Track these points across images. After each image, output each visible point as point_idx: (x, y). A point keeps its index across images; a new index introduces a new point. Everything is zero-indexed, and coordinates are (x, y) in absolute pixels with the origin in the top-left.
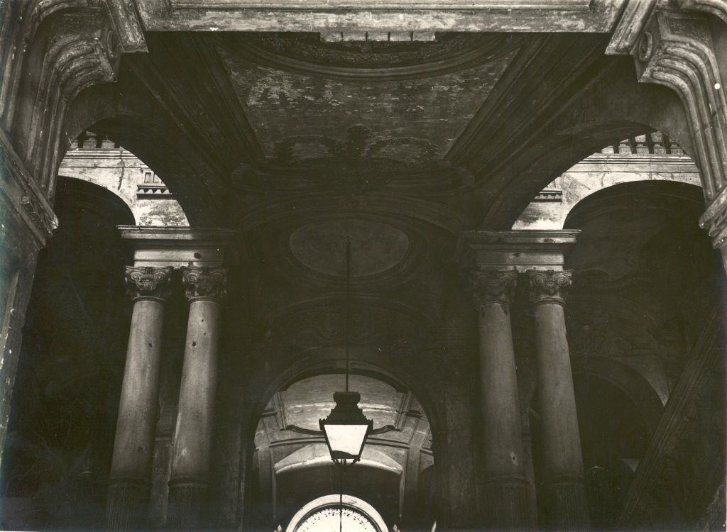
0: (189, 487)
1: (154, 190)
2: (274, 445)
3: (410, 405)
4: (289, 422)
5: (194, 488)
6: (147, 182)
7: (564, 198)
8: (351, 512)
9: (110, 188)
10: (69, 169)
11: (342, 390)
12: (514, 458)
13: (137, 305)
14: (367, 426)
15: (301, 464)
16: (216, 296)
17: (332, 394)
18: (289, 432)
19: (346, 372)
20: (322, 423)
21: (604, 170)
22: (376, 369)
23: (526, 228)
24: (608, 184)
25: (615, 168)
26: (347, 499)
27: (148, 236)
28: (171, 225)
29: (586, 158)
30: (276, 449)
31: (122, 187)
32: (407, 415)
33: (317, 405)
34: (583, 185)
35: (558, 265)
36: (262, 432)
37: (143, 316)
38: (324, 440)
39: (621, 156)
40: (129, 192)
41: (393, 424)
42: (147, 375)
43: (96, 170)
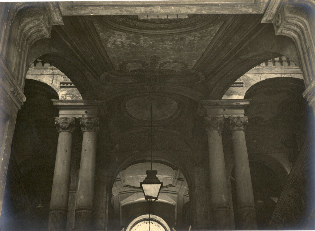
1: (67, 84)
2: (120, 193)
3: (179, 175)
4: (127, 184)
6: (64, 81)
7: (244, 85)
8: (154, 222)
9: (48, 84)
10: (30, 76)
11: (150, 169)
12: (224, 198)
13: (60, 134)
14: (160, 185)
15: (132, 201)
19: (151, 161)
20: (141, 184)
22: (164, 160)
23: (228, 98)
24: (263, 79)
26: (152, 216)
27: (65, 104)
28: (74, 99)
30: (121, 195)
31: (53, 83)
33: (139, 176)
37: (64, 139)
38: (142, 191)
39: (269, 67)
41: (171, 184)
42: (65, 165)
43: (42, 76)
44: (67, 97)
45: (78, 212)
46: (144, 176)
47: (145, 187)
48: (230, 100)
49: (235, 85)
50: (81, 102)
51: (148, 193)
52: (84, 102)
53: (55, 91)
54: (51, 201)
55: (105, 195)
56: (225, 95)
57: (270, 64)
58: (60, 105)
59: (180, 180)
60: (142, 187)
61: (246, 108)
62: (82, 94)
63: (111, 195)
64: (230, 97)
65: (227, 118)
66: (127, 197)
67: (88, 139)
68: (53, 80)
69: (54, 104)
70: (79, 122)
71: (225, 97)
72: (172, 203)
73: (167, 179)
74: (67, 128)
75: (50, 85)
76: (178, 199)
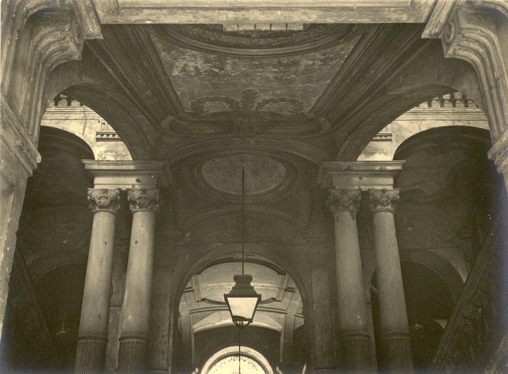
0: (133, 342)
1: (108, 135)
2: (192, 312)
4: (203, 296)
5: (137, 342)
7: (393, 138)
9: (77, 134)
12: (360, 320)
15: (211, 325)
16: (151, 209)
18: (203, 303)
19: (242, 261)
20: (226, 296)
23: (367, 160)
24: (424, 129)
26: (244, 349)
28: (119, 159)
29: (408, 110)
30: (194, 315)
31: (85, 133)
32: (285, 290)
40: (90, 137)
43: (67, 121)
47: (232, 301)
50: (129, 164)
51: (236, 313)
52: (135, 164)
57: (436, 105)
59: (288, 291)
60: (227, 303)
61: (396, 175)
70: (87, 198)
71: (362, 158)
74: (108, 207)
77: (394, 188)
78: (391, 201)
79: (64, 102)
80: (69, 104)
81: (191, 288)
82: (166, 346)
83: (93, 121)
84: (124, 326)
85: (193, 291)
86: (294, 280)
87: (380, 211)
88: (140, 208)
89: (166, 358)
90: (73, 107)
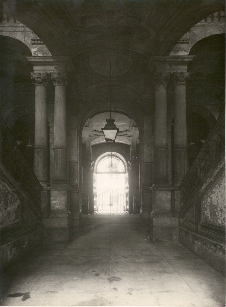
1: (38, 41)
2: (90, 136)
3: (133, 123)
4: (94, 129)
5: (61, 151)
6: (35, 38)
7: (190, 42)
8: (115, 157)
9: (21, 41)
10: (5, 33)
11: (109, 118)
13: (36, 88)
14: (117, 130)
15: (99, 142)
16: (63, 84)
17: (106, 119)
18: (94, 132)
19: (111, 111)
20: (102, 129)
21: (207, 29)
22: (121, 110)
23: (175, 55)
24: (207, 35)
25: (211, 28)
26: (113, 153)
27: (37, 60)
28: (45, 56)
29: (196, 24)
30: (91, 137)
31: (26, 40)
32: (132, 126)
33: (103, 123)
34: (198, 36)
35: (185, 70)
36: (86, 132)
37: (39, 91)
38: (103, 134)
39: (214, 22)
40: (29, 42)
41: (128, 129)
43: (15, 33)
44: (39, 54)
45: (56, 150)
46: (105, 123)
47: (106, 132)
48: (176, 56)
49: (182, 41)
50: (50, 59)
51: (107, 137)
53: (28, 47)
54: (36, 141)
55: (77, 138)
56: (172, 52)
57: (209, 20)
58: (33, 61)
59: (134, 126)
60: (103, 132)
61: (189, 64)
62: (50, 50)
63: (81, 138)
64: (177, 53)
65: (172, 74)
66: (95, 139)
67: (59, 93)
68: (25, 36)
69: (28, 60)
70: (31, 78)
71: (172, 54)
72: (128, 144)
73: (124, 125)
74: (41, 83)
75: (23, 41)
76: (132, 141)
77: (187, 72)
78: (185, 79)
79: (12, 20)
80: (15, 22)
81: (89, 125)
82: (77, 152)
83: (29, 32)
84: (55, 143)
85: (90, 126)
86: (136, 122)
87: (179, 85)
88: (58, 83)
89: (77, 157)
90: (17, 24)
